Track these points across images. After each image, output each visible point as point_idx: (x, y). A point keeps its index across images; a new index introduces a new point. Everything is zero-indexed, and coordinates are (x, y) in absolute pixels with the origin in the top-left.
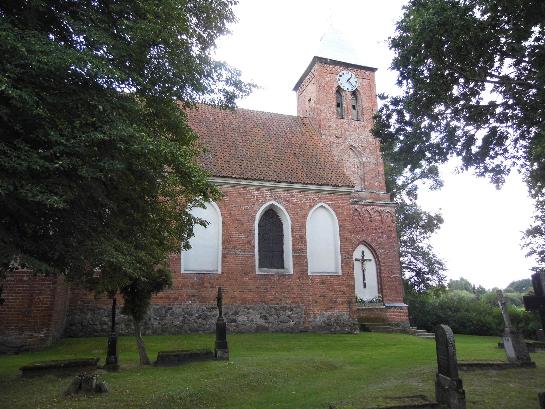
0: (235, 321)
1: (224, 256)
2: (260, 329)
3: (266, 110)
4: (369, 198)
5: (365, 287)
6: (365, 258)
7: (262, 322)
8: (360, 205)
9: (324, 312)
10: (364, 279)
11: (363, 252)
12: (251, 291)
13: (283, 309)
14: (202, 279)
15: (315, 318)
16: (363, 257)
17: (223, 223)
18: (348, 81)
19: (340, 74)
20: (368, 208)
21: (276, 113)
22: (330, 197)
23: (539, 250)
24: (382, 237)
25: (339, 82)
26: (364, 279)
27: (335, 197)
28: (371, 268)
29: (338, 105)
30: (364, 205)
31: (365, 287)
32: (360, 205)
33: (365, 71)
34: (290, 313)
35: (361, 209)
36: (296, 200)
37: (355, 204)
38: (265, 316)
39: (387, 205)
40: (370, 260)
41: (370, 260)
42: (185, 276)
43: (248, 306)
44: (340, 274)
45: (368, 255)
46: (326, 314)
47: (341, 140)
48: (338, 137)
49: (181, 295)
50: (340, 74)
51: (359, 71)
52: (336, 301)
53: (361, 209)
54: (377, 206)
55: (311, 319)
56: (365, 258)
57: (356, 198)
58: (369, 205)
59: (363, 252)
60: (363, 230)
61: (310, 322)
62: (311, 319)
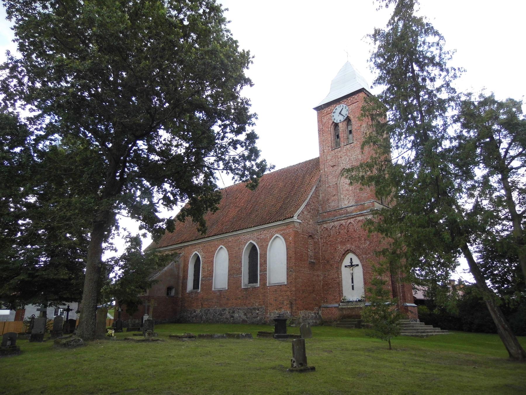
0: (233, 317)
1: (229, 280)
2: (244, 322)
3: (301, 162)
4: (355, 211)
5: (353, 289)
6: (353, 264)
7: (244, 317)
8: (344, 219)
9: (275, 311)
10: (353, 282)
11: (351, 259)
12: (240, 298)
13: (254, 309)
14: (220, 294)
15: (270, 315)
16: (351, 262)
17: (229, 259)
18: (340, 113)
19: (334, 111)
20: (352, 220)
21: (292, 165)
22: (282, 228)
23: (503, 229)
24: (365, 243)
25: (333, 118)
26: (353, 282)
27: (285, 227)
28: (359, 272)
29: (338, 136)
30: (348, 219)
31: (353, 289)
32: (344, 219)
33: (354, 96)
34: (258, 312)
35: (346, 223)
36: (262, 236)
37: (340, 220)
38: (246, 314)
39: (367, 213)
40: (357, 265)
41: (357, 265)
42: (214, 292)
43: (238, 308)
44: (286, 283)
45: (356, 261)
46: (277, 312)
47: (335, 168)
48: (333, 166)
49: (213, 302)
50: (334, 111)
51: (349, 99)
52: (283, 303)
53: (346, 223)
54: (359, 216)
55: (268, 316)
56: (353, 264)
57: (344, 214)
58: (353, 218)
59: (351, 259)
60: (348, 240)
61: (268, 318)
62: (268, 316)
